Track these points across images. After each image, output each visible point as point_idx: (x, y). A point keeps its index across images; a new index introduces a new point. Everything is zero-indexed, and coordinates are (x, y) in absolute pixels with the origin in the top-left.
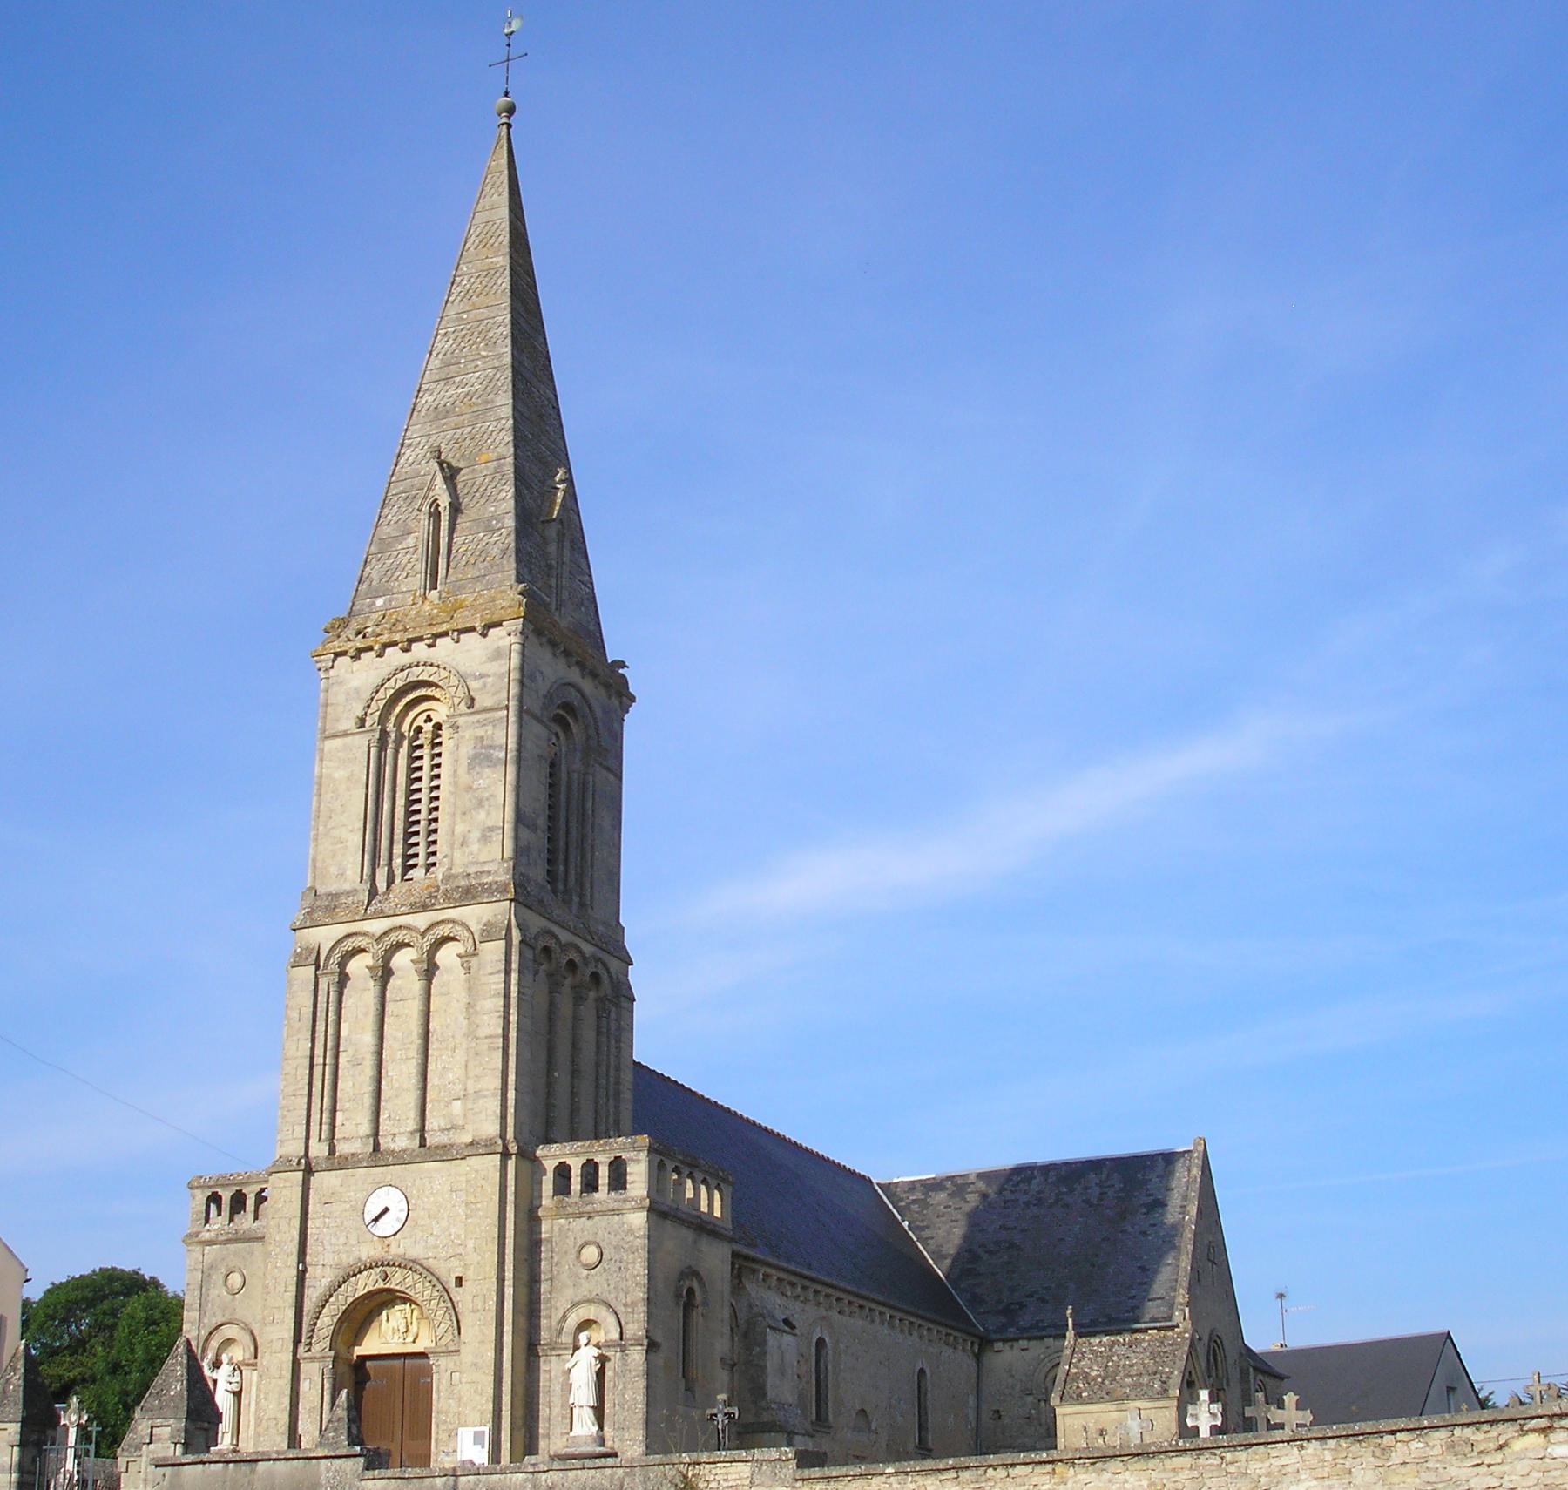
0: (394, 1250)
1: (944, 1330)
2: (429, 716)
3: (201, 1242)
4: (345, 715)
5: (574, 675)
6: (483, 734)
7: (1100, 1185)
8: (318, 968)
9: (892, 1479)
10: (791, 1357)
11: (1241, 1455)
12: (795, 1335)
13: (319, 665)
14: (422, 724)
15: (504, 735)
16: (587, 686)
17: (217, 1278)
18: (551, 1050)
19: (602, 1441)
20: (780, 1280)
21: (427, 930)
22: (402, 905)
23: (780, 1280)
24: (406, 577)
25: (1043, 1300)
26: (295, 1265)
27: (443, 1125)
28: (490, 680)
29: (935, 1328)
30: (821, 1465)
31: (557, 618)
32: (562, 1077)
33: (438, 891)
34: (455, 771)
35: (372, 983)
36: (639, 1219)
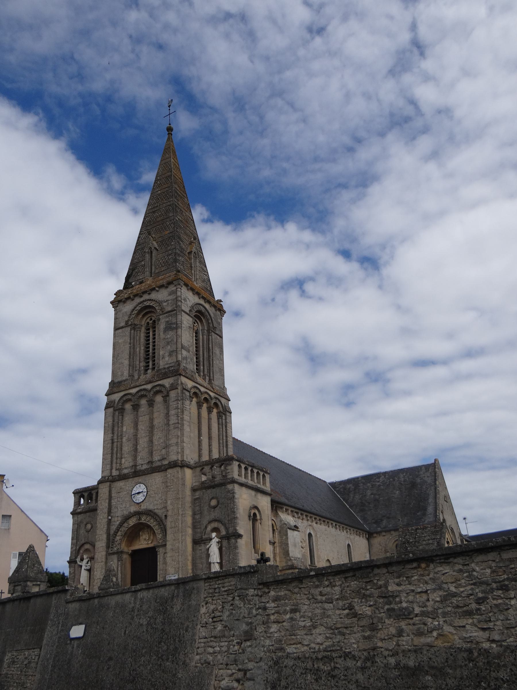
0: (142, 507)
2: (151, 318)
5: (202, 302)
10: (298, 540)
14: (149, 321)
16: (207, 306)
17: (83, 526)
27: (159, 458)
28: (170, 302)
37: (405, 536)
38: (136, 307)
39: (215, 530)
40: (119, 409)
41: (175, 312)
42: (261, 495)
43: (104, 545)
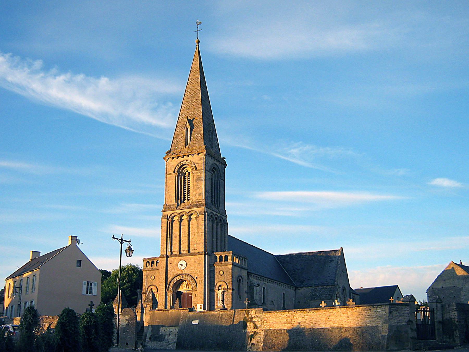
0: (184, 272)
1: (288, 285)
3: (145, 270)
4: (171, 170)
5: (215, 162)
6: (198, 175)
8: (167, 219)
9: (278, 313)
11: (332, 310)
12: (259, 287)
14: (186, 172)
15: (202, 175)
16: (218, 163)
18: (212, 235)
19: (224, 306)
20: (256, 277)
21: (189, 212)
22: (184, 208)
23: (256, 277)
24: (182, 143)
25: (308, 279)
26: (165, 275)
29: (286, 285)
30: (267, 311)
31: (212, 150)
32: (215, 239)
33: (190, 205)
34: (193, 182)
35: (178, 222)
36: (230, 267)
42: (243, 270)
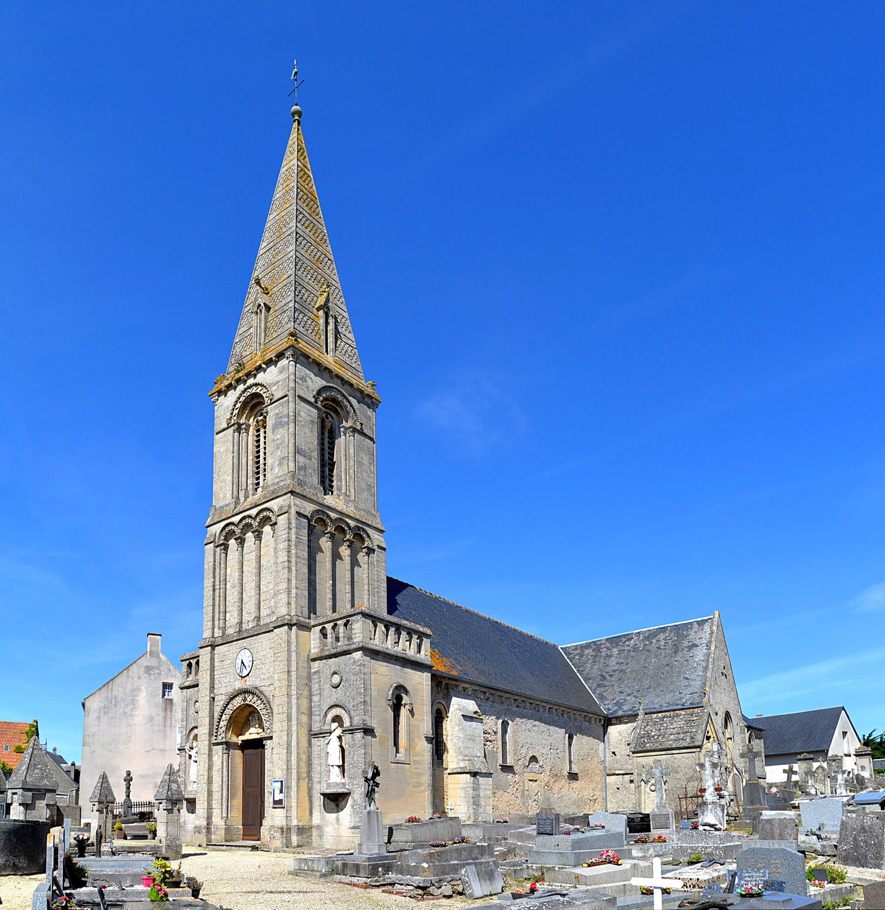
7: (665, 639)
13: (213, 400)
28: (280, 383)
37: (645, 727)
38: (239, 398)
39: (337, 719)
40: (221, 545)
41: (287, 398)
43: (207, 731)
